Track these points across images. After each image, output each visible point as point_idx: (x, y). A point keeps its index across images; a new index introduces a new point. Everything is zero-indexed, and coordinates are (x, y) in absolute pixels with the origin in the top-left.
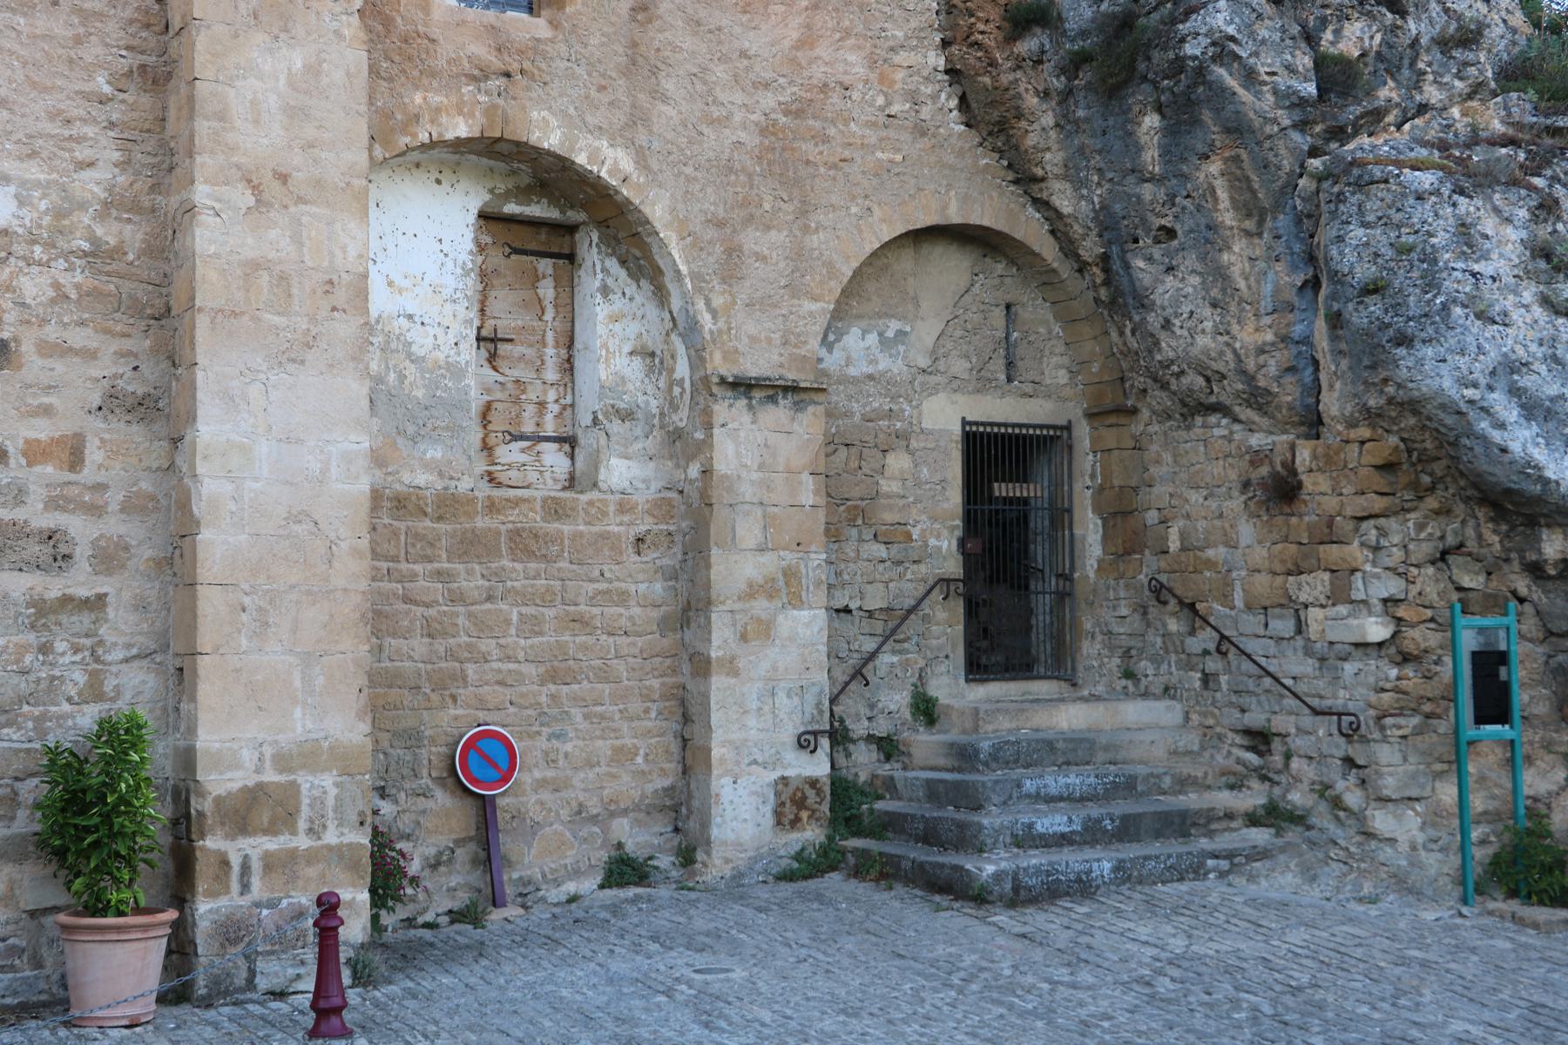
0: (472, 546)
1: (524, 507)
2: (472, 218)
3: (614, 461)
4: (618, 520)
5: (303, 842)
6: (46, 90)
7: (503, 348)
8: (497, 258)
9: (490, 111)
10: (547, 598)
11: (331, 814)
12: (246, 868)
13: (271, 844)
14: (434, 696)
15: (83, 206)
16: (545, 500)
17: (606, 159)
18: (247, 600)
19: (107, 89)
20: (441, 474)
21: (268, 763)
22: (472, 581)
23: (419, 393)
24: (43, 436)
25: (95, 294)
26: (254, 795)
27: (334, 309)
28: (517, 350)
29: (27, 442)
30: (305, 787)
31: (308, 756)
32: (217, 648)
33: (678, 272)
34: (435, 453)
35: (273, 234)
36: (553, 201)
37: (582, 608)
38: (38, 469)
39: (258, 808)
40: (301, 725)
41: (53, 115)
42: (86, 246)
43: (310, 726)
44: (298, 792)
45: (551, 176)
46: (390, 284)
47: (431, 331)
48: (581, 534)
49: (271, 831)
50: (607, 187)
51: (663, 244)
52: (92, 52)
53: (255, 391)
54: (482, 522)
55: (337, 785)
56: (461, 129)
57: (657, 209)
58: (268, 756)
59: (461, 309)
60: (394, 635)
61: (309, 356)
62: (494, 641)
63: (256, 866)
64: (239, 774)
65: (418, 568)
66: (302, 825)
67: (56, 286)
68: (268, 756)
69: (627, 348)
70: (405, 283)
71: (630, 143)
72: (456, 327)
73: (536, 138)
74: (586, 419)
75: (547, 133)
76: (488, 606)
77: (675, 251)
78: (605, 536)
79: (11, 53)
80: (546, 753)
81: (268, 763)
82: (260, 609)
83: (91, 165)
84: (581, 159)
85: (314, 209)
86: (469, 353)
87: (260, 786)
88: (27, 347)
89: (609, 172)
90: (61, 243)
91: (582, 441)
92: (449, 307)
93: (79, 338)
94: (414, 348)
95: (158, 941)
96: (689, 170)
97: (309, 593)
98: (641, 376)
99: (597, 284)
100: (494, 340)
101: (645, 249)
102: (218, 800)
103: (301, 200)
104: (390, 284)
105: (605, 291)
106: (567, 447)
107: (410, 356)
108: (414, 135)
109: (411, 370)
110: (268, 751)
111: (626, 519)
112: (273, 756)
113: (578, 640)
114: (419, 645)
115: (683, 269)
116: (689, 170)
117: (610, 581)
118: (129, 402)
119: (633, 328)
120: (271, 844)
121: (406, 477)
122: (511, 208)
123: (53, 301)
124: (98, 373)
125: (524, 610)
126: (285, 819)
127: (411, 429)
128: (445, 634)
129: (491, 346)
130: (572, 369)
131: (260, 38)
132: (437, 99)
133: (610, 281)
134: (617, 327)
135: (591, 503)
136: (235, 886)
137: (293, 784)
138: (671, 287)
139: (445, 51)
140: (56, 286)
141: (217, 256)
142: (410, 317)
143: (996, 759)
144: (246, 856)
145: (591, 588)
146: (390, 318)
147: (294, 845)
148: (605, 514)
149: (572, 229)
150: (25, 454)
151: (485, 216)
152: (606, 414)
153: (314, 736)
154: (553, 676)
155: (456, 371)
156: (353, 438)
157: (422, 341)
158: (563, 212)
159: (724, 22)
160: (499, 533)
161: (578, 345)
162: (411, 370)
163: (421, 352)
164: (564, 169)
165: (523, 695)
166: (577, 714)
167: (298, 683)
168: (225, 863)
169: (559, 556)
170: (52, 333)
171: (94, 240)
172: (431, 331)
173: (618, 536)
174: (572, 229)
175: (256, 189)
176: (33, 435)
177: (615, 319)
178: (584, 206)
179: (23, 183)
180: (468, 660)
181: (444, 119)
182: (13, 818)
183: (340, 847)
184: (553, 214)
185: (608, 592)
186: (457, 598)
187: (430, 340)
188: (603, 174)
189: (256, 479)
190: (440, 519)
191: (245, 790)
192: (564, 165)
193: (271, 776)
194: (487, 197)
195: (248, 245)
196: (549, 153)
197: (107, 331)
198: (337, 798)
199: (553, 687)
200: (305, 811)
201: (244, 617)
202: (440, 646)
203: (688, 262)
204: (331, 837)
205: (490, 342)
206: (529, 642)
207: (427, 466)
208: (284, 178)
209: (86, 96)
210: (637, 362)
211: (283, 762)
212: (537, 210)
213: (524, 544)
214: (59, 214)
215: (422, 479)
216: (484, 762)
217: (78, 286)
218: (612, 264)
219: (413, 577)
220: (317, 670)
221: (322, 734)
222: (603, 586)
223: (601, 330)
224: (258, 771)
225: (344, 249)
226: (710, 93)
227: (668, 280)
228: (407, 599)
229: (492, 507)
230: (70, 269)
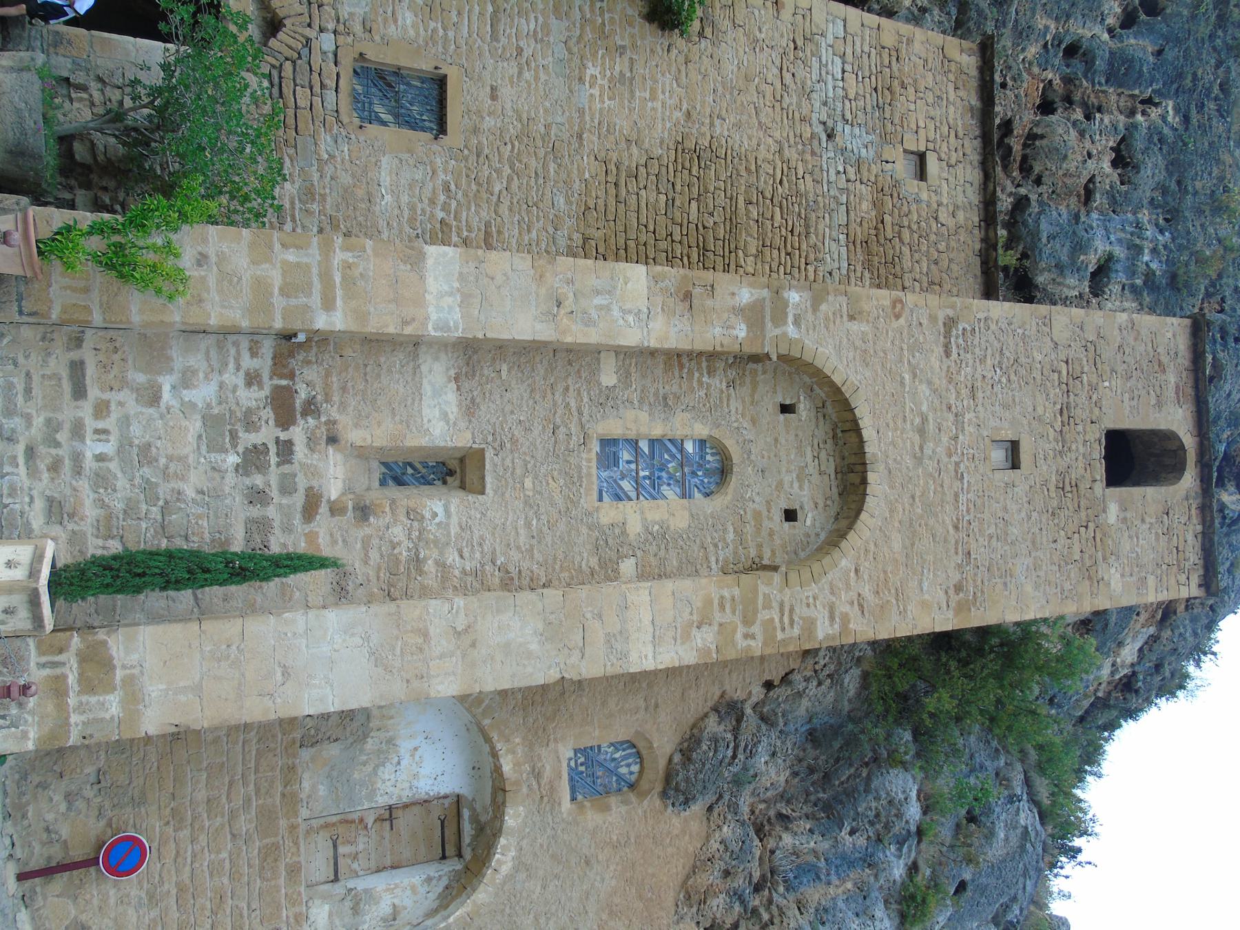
0: (267, 818)
1: (294, 850)
2: (457, 791)
3: (327, 907)
4: (290, 914)
5: (72, 701)
6: (493, 534)
7: (387, 824)
8: (437, 812)
9: (517, 783)
10: (234, 876)
11: (91, 717)
12: (55, 665)
13: (72, 679)
14: (168, 810)
15: (441, 553)
16: (299, 862)
17: (504, 857)
18: (234, 647)
19: (499, 563)
20: (309, 796)
21: (128, 671)
22: (244, 824)
23: (356, 776)
24: (320, 540)
25: (398, 561)
26: (107, 665)
27: (408, 681)
28: (387, 834)
29: (317, 533)
30: (110, 697)
31: (133, 696)
32: (204, 632)
33: (449, 916)
34: (322, 790)
35: (444, 642)
36: (475, 838)
37: (230, 902)
38: (303, 538)
39: (97, 668)
40: (154, 689)
41: (481, 537)
42: (422, 556)
43: (153, 695)
44: (108, 693)
45: (488, 833)
46: (416, 749)
47: (392, 777)
48: (278, 891)
49: (82, 678)
50: (490, 861)
51: (462, 904)
52: (515, 555)
53: (359, 641)
54: (283, 823)
55: (112, 718)
56: (507, 767)
57: (482, 895)
58: (133, 671)
59: (407, 793)
60: (208, 777)
61: (380, 670)
62: (205, 844)
63: (58, 671)
64: (122, 655)
65: (252, 787)
66: (84, 698)
67: (399, 544)
68: (133, 671)
69: (396, 901)
70: (417, 758)
71: (516, 869)
72: (396, 791)
73: (509, 811)
74: (351, 884)
75: (513, 818)
76: (229, 837)
77: (459, 912)
78: (279, 908)
79: (507, 519)
80: (128, 896)
81: (128, 671)
82: (228, 657)
83: (461, 557)
84: (502, 841)
85: (460, 663)
86: (382, 801)
87: (114, 667)
88: (368, 531)
89: (498, 860)
90: (421, 544)
91: (337, 885)
92: (407, 785)
93: (374, 555)
94: (382, 768)
95: (20, 268)
96: (508, 910)
97: (240, 684)
98: (381, 914)
99: (432, 874)
100: (391, 819)
101: (459, 895)
102: (104, 643)
103: (464, 656)
104: (416, 749)
105: (429, 880)
106: (332, 878)
107: (376, 767)
108: (498, 741)
109: (369, 768)
110: (136, 671)
111: (292, 920)
112: (133, 675)
113: (208, 903)
114: (201, 795)
115: (451, 920)
116: (508, 910)
117: (249, 916)
118: (343, 583)
119: (408, 902)
120: (72, 679)
121: (306, 776)
122: (466, 813)
123: (391, 542)
124: (357, 566)
125: (227, 861)
126: (88, 686)
127: (335, 774)
128: (209, 812)
129: (387, 816)
130: (378, 871)
131: (540, 626)
132: (519, 750)
133: (434, 882)
134: (409, 892)
135: (300, 894)
136: (44, 659)
137: (115, 689)
138: (438, 917)
139: (544, 752)
140: (399, 544)
141: (428, 613)
142: (399, 763)
143: (168, 582)
144: (64, 664)
145: (244, 905)
146: (397, 752)
147: (71, 694)
148: (294, 905)
149: (460, 856)
150: (311, 532)
151: (459, 798)
152: (356, 895)
153: (147, 698)
154: (181, 889)
155: (371, 795)
156: (336, 701)
157: (386, 772)
158: (469, 845)
159: (591, 915)
160: (276, 835)
161: (394, 872)
162: (369, 768)
163: (380, 773)
164: (494, 835)
165: (169, 871)
166: (154, 913)
167: (182, 684)
168: (61, 651)
169: (263, 879)
170: (375, 542)
171: (426, 559)
172: (392, 777)
173: (279, 917)
174: (460, 856)
175: (466, 630)
176: (321, 535)
177: (413, 889)
178: (474, 856)
179: (448, 525)
180: (193, 828)
181: (510, 757)
182: (97, 537)
183: (69, 725)
184: (467, 839)
185: (241, 916)
186: (233, 815)
187: (387, 777)
188: (497, 856)
189: (307, 646)
190: (283, 795)
191: (111, 658)
192: (497, 833)
193: (119, 674)
194: (470, 798)
195: (436, 629)
196: (502, 821)
197: (379, 569)
198: (102, 720)
199: (174, 892)
200: (94, 700)
201: (224, 647)
202: (202, 809)
203: (455, 922)
204: (74, 718)
205: (390, 815)
206: (206, 869)
207: (314, 787)
208: (473, 645)
209: (494, 552)
210: (389, 910)
211: (129, 681)
212: (468, 829)
213: (270, 854)
214: (436, 542)
215: (306, 785)
216: (144, 535)
217: (401, 554)
218: (445, 881)
219: (245, 784)
220: (191, 696)
221: (147, 703)
222: (245, 913)
223: (406, 881)
224: (124, 667)
225: (442, 683)
226: (552, 914)
227: (445, 913)
228: (231, 784)
229: (293, 827)
230: (409, 550)
